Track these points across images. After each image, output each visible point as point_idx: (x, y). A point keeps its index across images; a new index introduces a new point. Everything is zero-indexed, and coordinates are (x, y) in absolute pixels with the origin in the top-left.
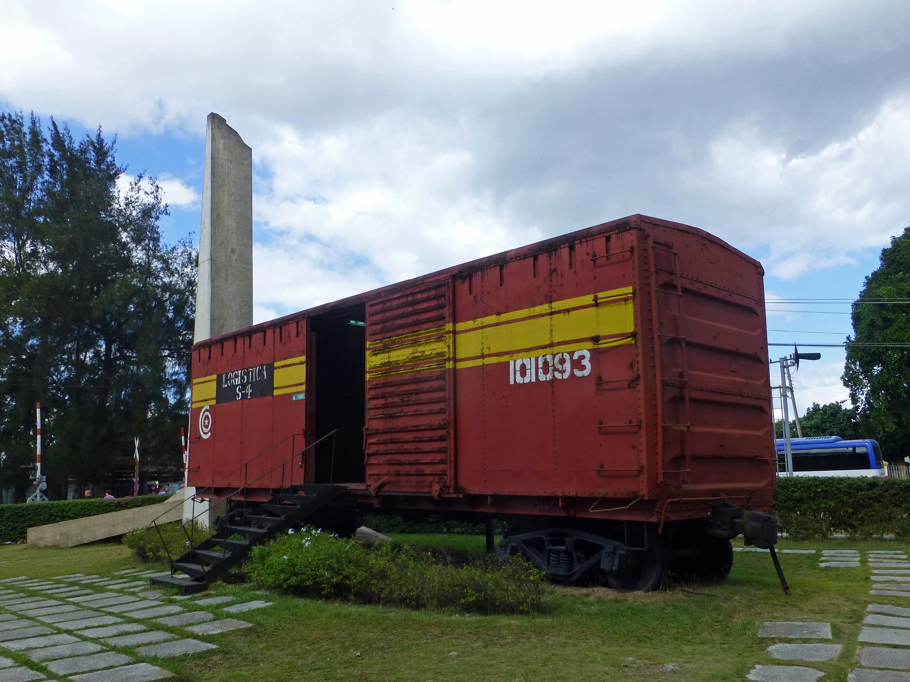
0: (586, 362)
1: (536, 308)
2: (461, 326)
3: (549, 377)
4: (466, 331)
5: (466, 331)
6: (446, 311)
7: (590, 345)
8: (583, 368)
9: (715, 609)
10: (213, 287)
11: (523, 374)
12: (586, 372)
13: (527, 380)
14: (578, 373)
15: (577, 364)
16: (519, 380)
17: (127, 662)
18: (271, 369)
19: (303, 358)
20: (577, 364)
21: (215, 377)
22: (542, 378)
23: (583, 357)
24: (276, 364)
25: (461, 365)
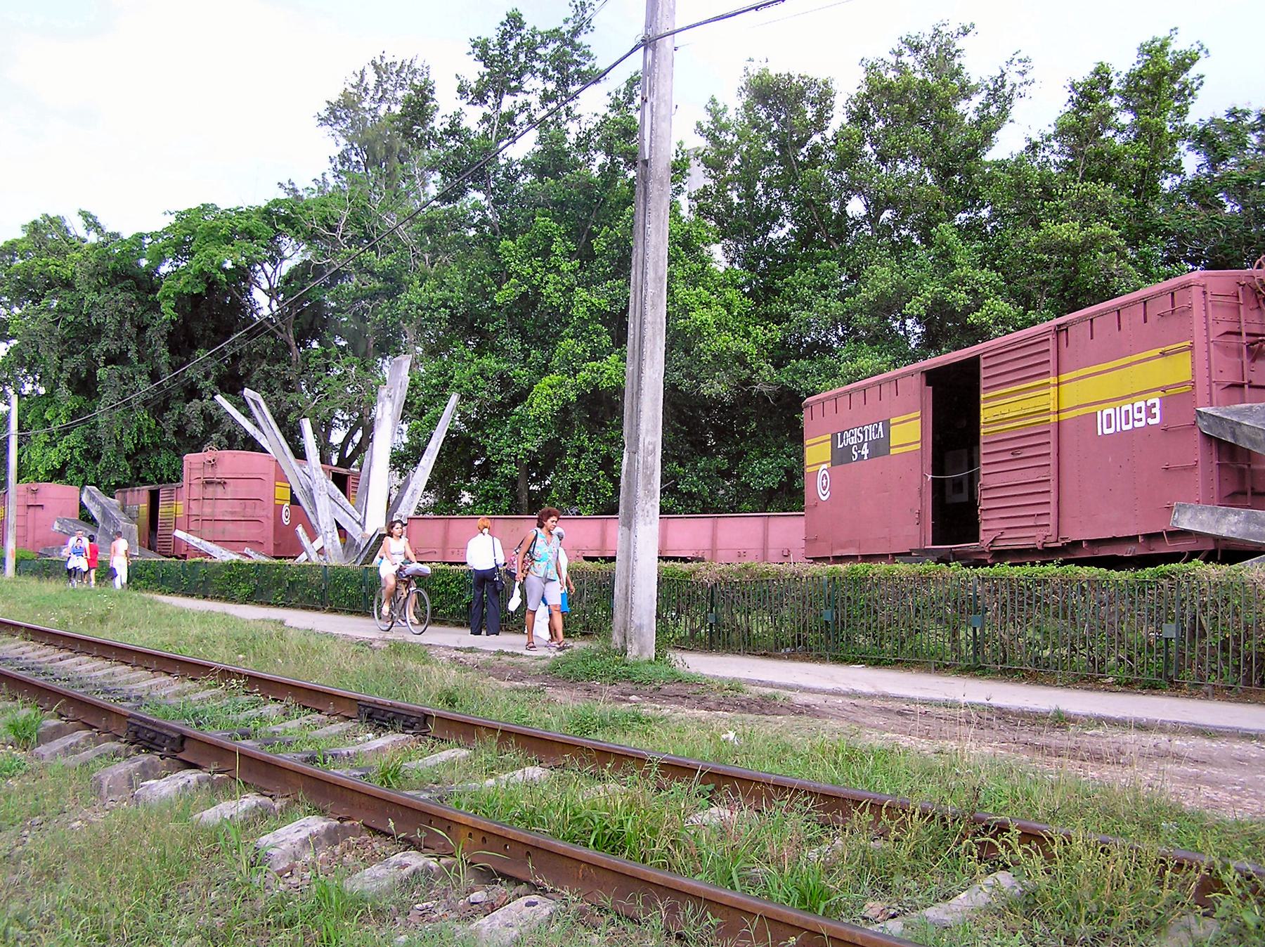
0: (1156, 410)
1: (15, 653)
2: (1063, 378)
3: (1129, 427)
4: (1070, 381)
5: (1070, 381)
6: (1052, 367)
7: (1160, 393)
8: (1154, 416)
9: (616, 301)
10: (854, 662)
12: (1157, 421)
13: (1111, 431)
14: (1151, 421)
15: (1150, 415)
16: (1107, 431)
17: (771, 544)
18: (887, 426)
19: (918, 414)
21: (829, 436)
22: (1125, 428)
23: (1154, 405)
24: (497, 542)
25: (1063, 416)
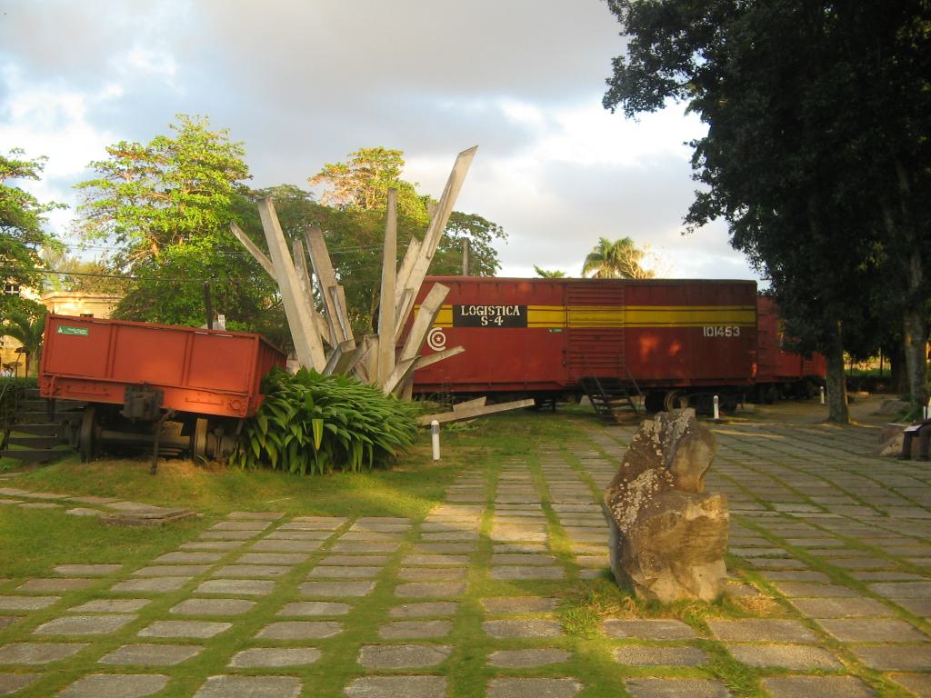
0: (738, 331)
11: (710, 333)
20: (734, 331)
